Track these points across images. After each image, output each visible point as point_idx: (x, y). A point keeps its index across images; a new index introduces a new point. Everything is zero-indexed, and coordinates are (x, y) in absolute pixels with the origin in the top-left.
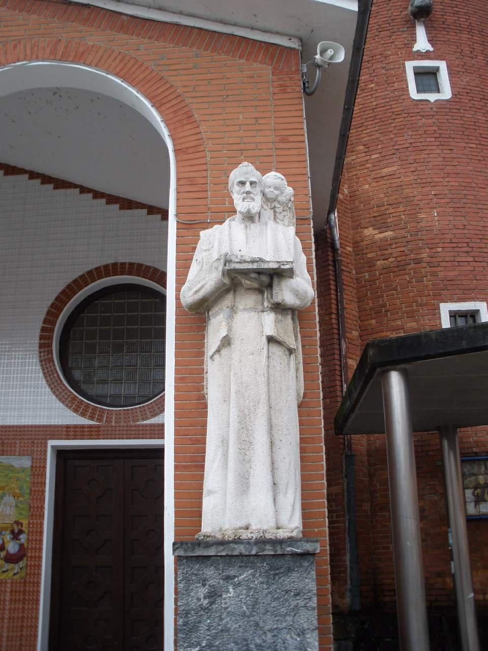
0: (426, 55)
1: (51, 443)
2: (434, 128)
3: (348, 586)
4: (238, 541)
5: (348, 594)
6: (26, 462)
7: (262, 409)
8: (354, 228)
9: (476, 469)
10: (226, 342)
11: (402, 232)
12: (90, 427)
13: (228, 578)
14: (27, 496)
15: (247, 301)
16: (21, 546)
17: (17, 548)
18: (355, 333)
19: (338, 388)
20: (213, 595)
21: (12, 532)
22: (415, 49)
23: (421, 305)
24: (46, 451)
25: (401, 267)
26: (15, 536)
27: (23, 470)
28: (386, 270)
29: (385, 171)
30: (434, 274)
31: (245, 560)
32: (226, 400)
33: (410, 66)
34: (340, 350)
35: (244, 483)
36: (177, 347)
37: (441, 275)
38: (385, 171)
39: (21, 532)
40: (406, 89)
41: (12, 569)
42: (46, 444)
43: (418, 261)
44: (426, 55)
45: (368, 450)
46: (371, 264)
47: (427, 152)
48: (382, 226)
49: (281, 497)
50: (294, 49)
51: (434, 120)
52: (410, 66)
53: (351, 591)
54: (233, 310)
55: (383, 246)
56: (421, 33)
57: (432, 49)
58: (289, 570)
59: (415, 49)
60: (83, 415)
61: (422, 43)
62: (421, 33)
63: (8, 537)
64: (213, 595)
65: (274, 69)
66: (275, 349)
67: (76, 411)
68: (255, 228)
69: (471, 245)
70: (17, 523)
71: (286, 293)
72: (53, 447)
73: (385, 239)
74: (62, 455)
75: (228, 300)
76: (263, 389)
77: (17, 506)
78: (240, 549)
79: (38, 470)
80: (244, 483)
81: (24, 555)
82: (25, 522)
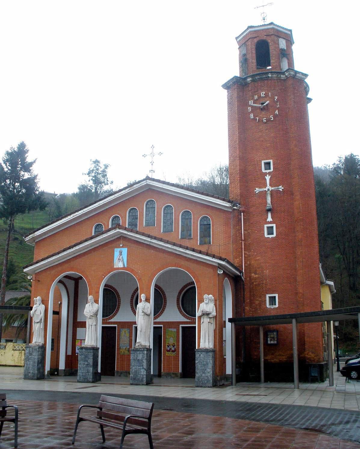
0: (270, 223)
1: (181, 325)
2: (270, 246)
3: (243, 358)
4: (203, 349)
5: (242, 360)
6: (175, 330)
7: (207, 332)
8: (250, 273)
9: (271, 334)
10: (203, 322)
11: (260, 276)
12: (189, 322)
13: (202, 353)
14: (176, 338)
15: (205, 317)
16: (175, 349)
17: (174, 349)
18: (248, 301)
19: (242, 314)
20: (200, 355)
21: (173, 346)
22: (267, 221)
23: (262, 295)
24: (133, 327)
25: (259, 284)
26: (174, 346)
27: (175, 332)
28: (256, 285)
29: (257, 258)
30: (266, 287)
31: (204, 351)
32: (203, 330)
33: (266, 226)
34: (243, 305)
35: (205, 342)
36: (198, 321)
37: (267, 287)
38: (257, 258)
39: (175, 345)
40: (264, 234)
41: (78, 437)
42: (179, 326)
43: (263, 284)
44: (270, 223)
45: (250, 329)
46: (253, 283)
47: (268, 253)
48: (256, 274)
49: (210, 343)
50: (217, 266)
51: (270, 243)
52: (266, 226)
53: (243, 359)
54: (204, 318)
55: (256, 278)
56: (269, 215)
57: (272, 220)
58: (208, 353)
59: (267, 221)
60: (188, 319)
61: (270, 219)
62: (269, 215)
63: (172, 347)
64: (200, 355)
65: (213, 270)
66: (209, 323)
67: (186, 318)
68: (207, 305)
69: (276, 279)
70: (174, 343)
71: (211, 316)
72: (181, 326)
73: (256, 277)
74: (183, 327)
75: (203, 317)
76: (208, 329)
77: (173, 340)
78: (203, 350)
79: (178, 332)
80: (205, 342)
81: (175, 351)
82: (176, 343)
